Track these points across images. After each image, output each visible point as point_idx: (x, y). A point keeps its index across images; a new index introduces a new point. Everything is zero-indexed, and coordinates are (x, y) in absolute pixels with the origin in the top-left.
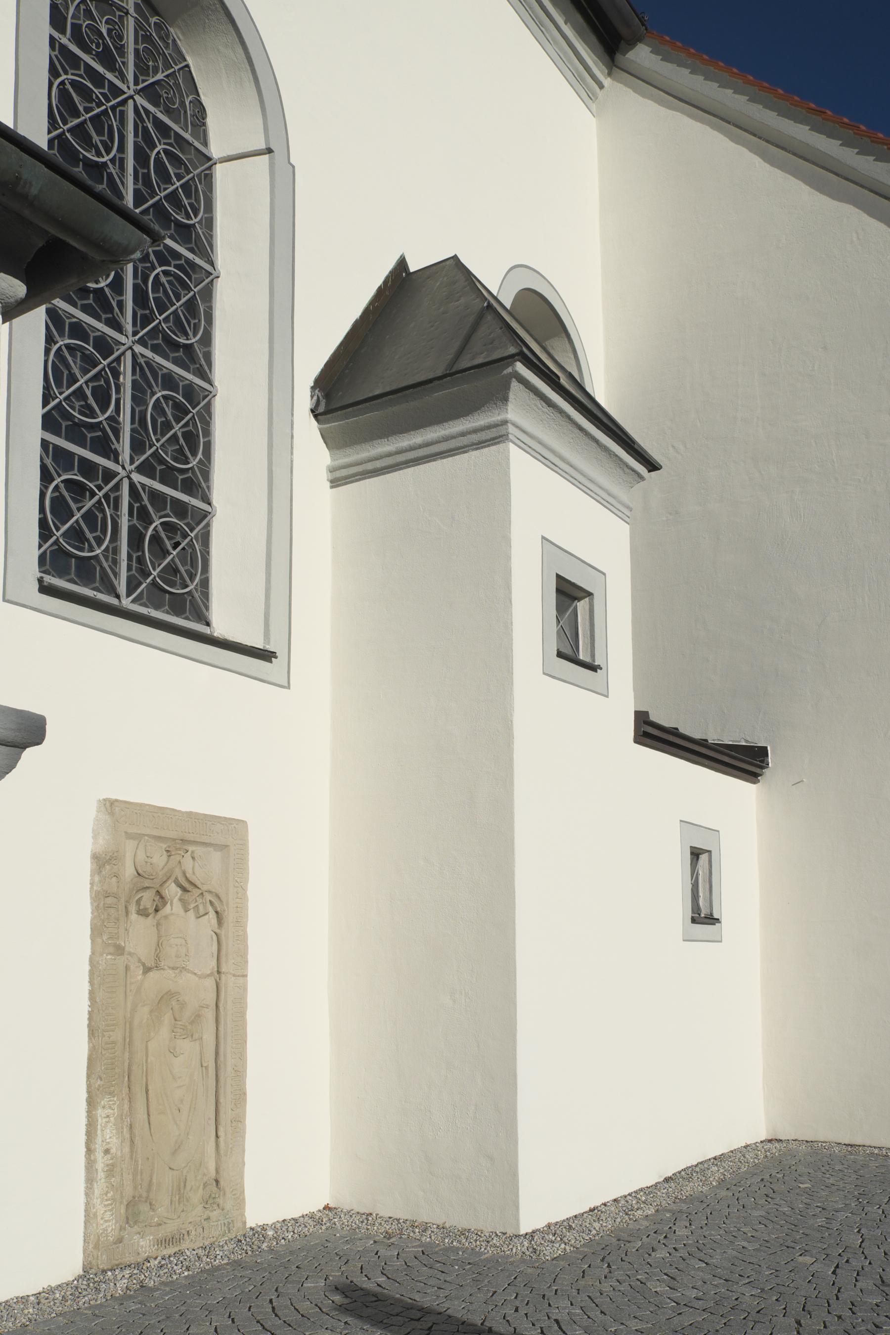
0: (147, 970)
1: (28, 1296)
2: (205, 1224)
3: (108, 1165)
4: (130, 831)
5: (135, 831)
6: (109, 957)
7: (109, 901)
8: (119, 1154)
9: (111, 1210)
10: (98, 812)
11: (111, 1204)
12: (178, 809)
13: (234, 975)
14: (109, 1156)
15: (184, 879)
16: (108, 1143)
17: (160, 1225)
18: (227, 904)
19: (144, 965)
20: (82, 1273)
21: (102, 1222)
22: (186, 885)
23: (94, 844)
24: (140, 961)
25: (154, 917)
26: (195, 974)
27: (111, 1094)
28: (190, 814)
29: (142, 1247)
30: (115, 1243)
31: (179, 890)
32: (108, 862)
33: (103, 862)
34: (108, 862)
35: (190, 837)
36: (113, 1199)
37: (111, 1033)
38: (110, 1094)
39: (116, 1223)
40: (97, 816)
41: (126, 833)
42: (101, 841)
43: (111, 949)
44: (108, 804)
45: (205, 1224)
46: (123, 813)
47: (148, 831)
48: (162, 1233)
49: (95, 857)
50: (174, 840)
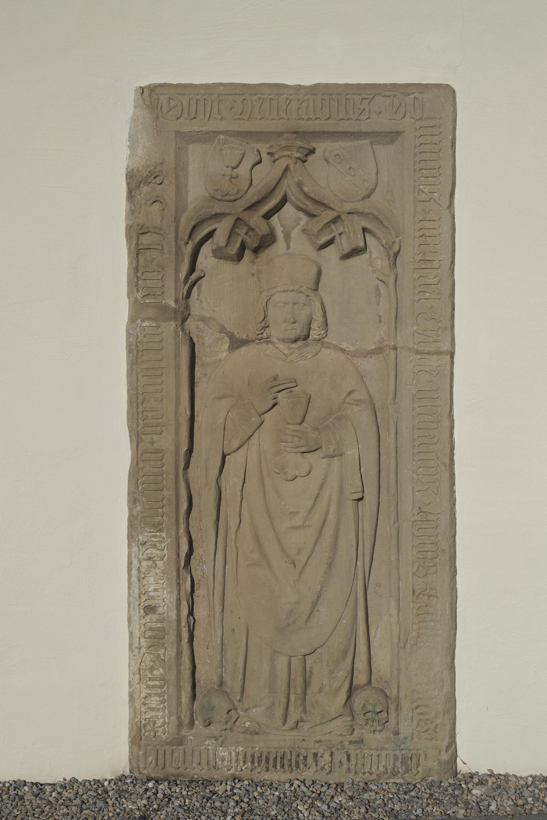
0: (237, 343)
2: (353, 750)
3: (151, 629)
4: (186, 129)
5: (196, 128)
9: (159, 695)
10: (135, 107)
12: (382, 82)
14: (154, 617)
15: (302, 198)
16: (153, 598)
17: (257, 734)
19: (231, 336)
20: (80, 780)
21: (143, 708)
22: (311, 207)
23: (131, 156)
24: (223, 329)
25: (253, 262)
26: (343, 350)
27: (158, 527)
28: (316, 90)
30: (169, 744)
31: (302, 215)
32: (146, 181)
34: (146, 181)
35: (313, 126)
37: (156, 437)
38: (154, 526)
40: (134, 114)
42: (140, 152)
43: (152, 312)
44: (146, 92)
45: (353, 750)
47: (222, 126)
48: (259, 745)
49: (130, 176)
50: (280, 134)
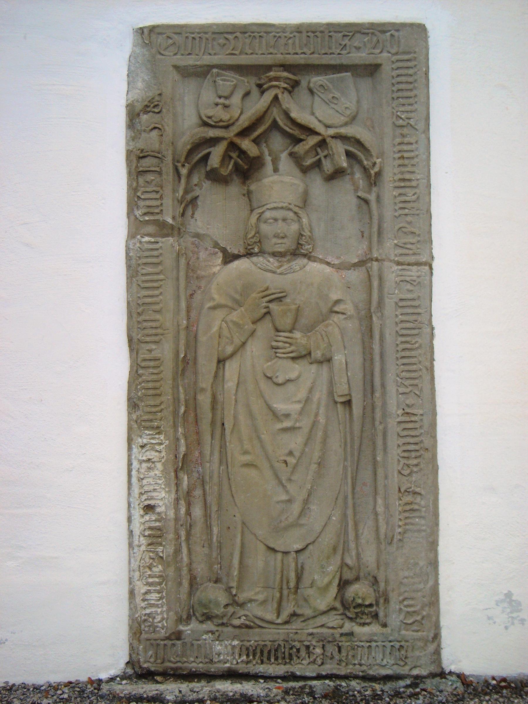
1: (100, 681)
2: (345, 643)
3: (150, 528)
5: (191, 62)
6: (147, 239)
7: (146, 163)
8: (171, 514)
11: (160, 584)
13: (399, 263)
18: (381, 155)
19: (224, 251)
21: (143, 604)
22: (296, 132)
24: (216, 245)
29: (219, 654)
33: (142, 114)
36: (163, 578)
39: (169, 610)
41: (176, 67)
42: (140, 85)
46: (170, 41)
47: (216, 60)
48: (254, 638)
